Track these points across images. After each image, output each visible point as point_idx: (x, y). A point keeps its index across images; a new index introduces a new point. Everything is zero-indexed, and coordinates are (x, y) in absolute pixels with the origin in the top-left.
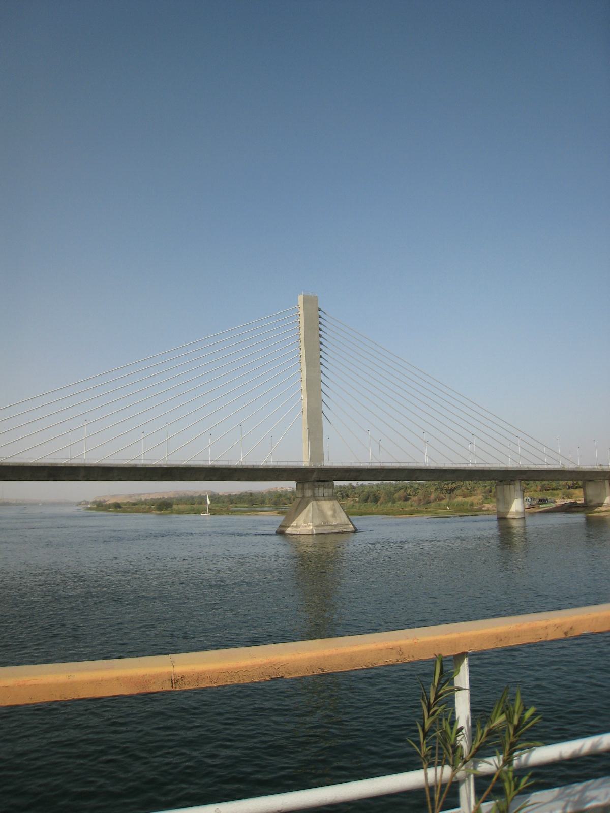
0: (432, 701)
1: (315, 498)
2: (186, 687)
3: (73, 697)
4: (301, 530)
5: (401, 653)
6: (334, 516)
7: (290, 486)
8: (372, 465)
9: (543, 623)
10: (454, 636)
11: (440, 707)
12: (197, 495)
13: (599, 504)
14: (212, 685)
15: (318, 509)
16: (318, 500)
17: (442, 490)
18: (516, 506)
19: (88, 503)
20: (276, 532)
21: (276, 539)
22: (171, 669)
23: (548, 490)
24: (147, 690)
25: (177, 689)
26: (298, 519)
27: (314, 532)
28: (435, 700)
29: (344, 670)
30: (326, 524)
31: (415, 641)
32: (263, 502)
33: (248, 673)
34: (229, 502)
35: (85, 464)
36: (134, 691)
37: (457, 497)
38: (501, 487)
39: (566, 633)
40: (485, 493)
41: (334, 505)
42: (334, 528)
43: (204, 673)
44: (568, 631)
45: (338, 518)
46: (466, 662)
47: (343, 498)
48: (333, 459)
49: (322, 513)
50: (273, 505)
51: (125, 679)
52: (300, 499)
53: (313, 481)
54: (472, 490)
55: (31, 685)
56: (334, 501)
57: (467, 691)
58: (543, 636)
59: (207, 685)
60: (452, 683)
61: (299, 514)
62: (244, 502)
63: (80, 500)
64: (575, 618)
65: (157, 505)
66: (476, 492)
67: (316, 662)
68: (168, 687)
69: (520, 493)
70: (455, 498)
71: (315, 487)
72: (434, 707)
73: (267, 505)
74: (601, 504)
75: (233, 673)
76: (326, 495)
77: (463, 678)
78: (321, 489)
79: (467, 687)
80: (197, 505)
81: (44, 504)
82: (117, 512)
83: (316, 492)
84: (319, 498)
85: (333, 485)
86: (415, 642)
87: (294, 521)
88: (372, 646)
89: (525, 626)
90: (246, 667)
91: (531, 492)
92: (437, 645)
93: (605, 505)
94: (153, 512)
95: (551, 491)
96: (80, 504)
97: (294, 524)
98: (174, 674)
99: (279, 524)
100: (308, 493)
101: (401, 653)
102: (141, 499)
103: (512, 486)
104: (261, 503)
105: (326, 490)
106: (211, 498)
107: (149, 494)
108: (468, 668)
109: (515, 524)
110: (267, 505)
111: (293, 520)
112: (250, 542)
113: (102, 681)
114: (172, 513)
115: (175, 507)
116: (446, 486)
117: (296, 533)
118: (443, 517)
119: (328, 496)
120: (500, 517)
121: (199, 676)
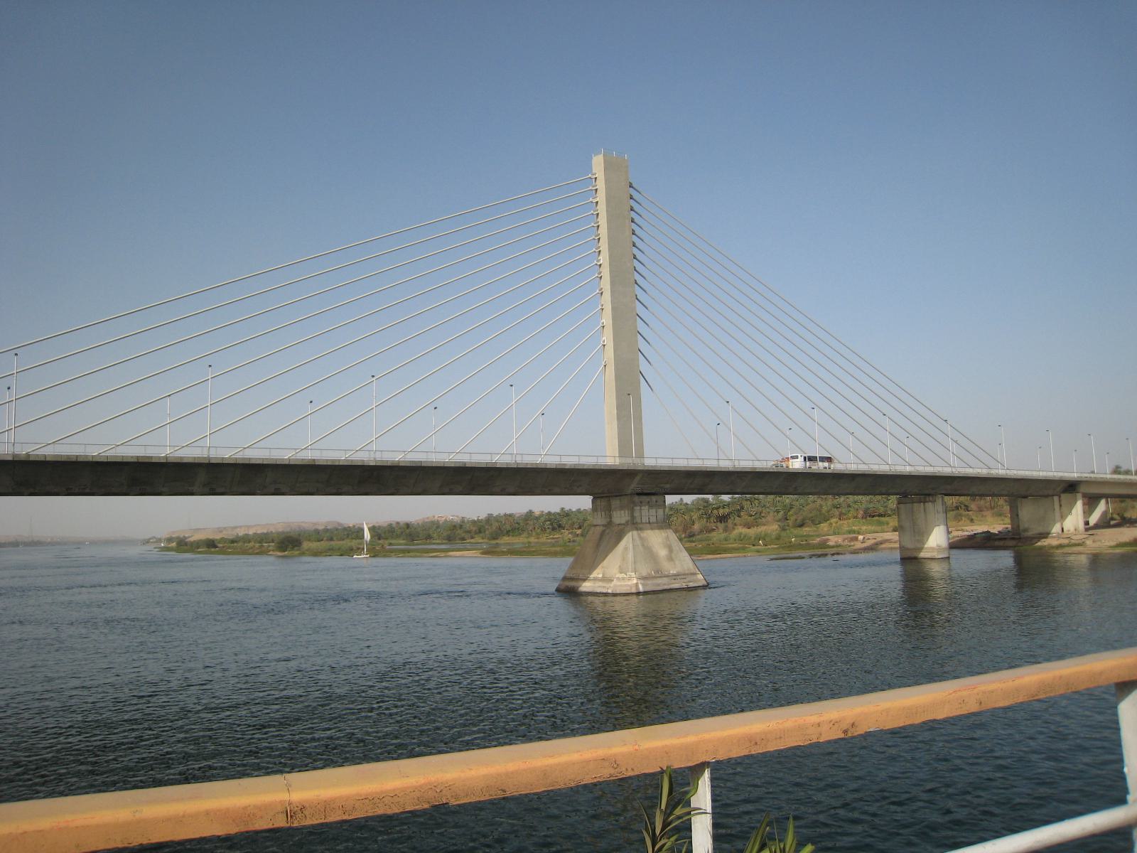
0: (658, 831)
1: (634, 525)
2: (308, 822)
3: (140, 843)
4: (615, 586)
5: (615, 766)
6: (670, 559)
7: (582, 503)
8: (736, 463)
9: (814, 719)
10: (691, 739)
11: (669, 838)
12: (385, 525)
13: (1040, 534)
14: (346, 817)
15: (643, 545)
16: (641, 529)
17: (709, 518)
18: (937, 539)
19: (159, 540)
20: (558, 590)
21: (559, 602)
22: (284, 796)
23: (873, 516)
24: (251, 828)
25: (295, 825)
26: (605, 563)
27: (641, 589)
28: (663, 829)
29: (535, 791)
30: (659, 574)
31: (637, 747)
32: (429, 537)
33: (399, 799)
34: (376, 538)
35: (209, 458)
36: (233, 829)
37: (736, 527)
38: (909, 506)
39: (845, 732)
40: (779, 521)
41: (667, 538)
42: (673, 581)
43: (333, 800)
44: (848, 729)
45: (677, 562)
46: (707, 775)
47: (554, 529)
48: (665, 448)
49: (651, 555)
50: (444, 541)
51: (218, 813)
52: (600, 529)
53: (631, 494)
54: (758, 516)
55: (77, 827)
56: (668, 530)
57: (709, 815)
58: (814, 737)
59: (338, 818)
60: (688, 803)
61: (606, 556)
62: (398, 537)
63: (147, 537)
64: (858, 710)
65: (278, 543)
66: (764, 520)
67: (495, 780)
68: (281, 822)
69: (942, 516)
70: (734, 529)
71: (634, 504)
72: (660, 840)
73: (434, 541)
74: (1045, 535)
75: (376, 799)
76: (653, 519)
77: (703, 796)
78: (645, 508)
79: (709, 810)
80: (327, 542)
81: (94, 543)
82: (212, 553)
83: (637, 514)
84: (641, 526)
85: (665, 502)
86: (636, 750)
87: (595, 569)
88: (575, 757)
89: (789, 724)
90: (394, 790)
91: (850, 519)
92: (667, 753)
93: (1054, 537)
94: (271, 553)
95: (877, 518)
96: (147, 542)
97: (597, 573)
98: (290, 804)
99: (561, 575)
100: (620, 517)
101: (615, 766)
102: (238, 534)
103: (929, 505)
104: (426, 539)
105: (653, 512)
106: (372, 529)
107: (249, 527)
108: (709, 783)
109: (936, 569)
110: (434, 541)
111: (593, 567)
112: (500, 606)
113: (184, 816)
114: (303, 554)
115: (306, 545)
116: (715, 511)
117: (604, 591)
118: (781, 559)
119: (657, 522)
120: (906, 556)
121: (327, 805)
